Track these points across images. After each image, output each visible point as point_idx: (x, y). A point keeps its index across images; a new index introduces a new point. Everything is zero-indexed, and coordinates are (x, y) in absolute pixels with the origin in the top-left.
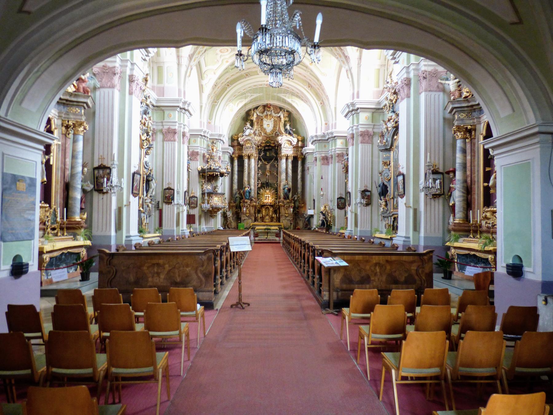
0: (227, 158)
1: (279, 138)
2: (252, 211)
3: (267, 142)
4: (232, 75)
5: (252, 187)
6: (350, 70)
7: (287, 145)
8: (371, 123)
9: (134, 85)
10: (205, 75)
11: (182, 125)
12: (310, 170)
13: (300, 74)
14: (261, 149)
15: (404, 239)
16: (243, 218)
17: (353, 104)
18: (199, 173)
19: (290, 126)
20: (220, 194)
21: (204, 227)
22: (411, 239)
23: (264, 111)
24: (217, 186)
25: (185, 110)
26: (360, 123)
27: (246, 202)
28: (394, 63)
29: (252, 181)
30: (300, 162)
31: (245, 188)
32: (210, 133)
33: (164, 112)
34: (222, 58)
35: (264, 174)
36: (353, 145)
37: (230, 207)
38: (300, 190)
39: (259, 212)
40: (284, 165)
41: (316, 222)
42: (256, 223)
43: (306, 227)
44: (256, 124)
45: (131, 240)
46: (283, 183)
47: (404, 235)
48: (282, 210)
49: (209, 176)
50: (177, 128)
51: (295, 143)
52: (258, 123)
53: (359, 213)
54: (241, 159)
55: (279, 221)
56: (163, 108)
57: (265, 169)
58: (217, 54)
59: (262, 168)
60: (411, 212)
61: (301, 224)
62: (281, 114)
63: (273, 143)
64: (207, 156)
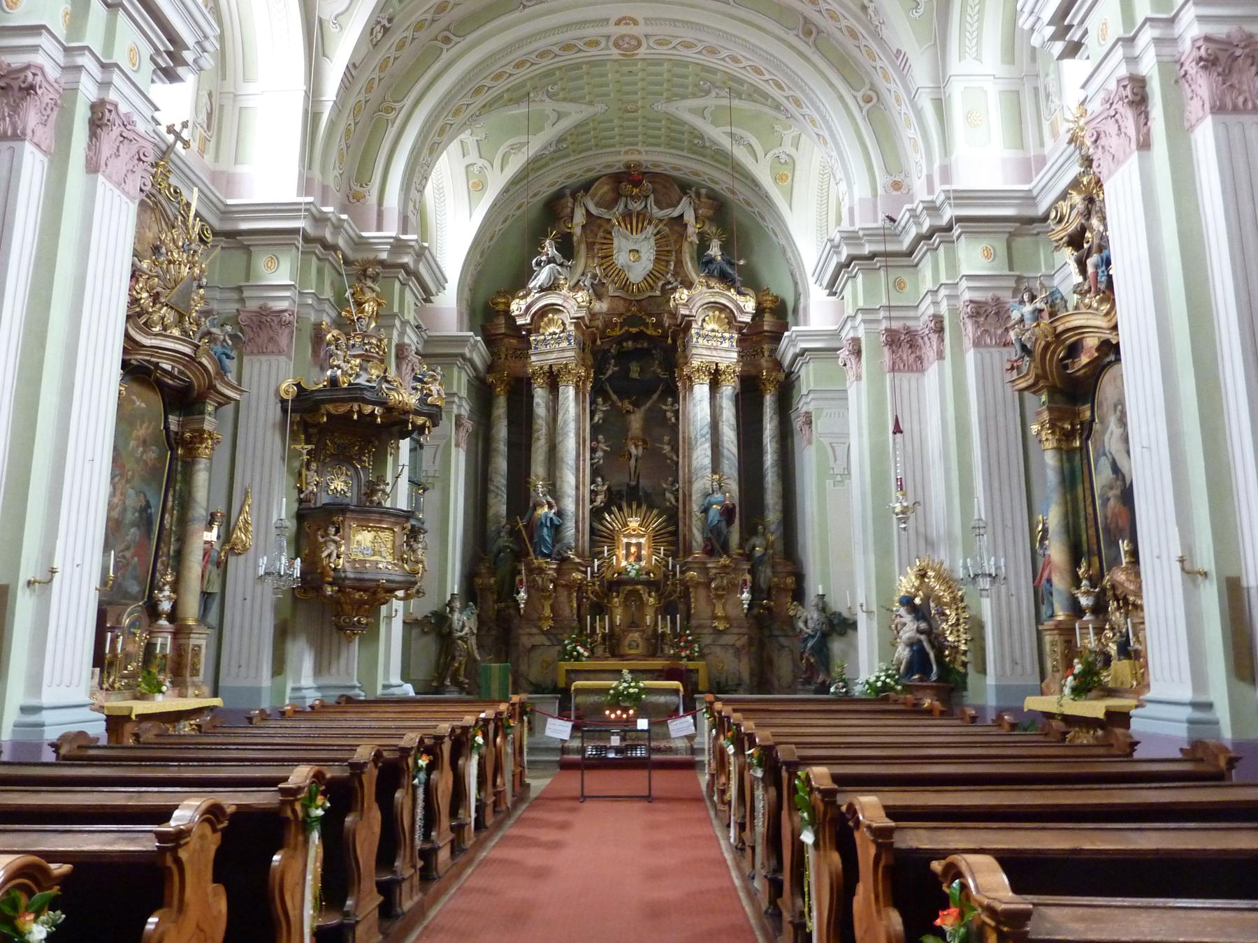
0: (461, 381)
2: (569, 607)
3: (630, 320)
5: (569, 505)
9: (109, 139)
12: (819, 425)
15: (1187, 712)
16: (526, 641)
19: (722, 248)
22: (1222, 712)
23: (615, 202)
27: (541, 571)
29: (571, 486)
31: (535, 509)
33: (249, 254)
35: (617, 453)
36: (1144, 144)
37: (471, 592)
38: (773, 516)
41: (868, 661)
43: (808, 681)
46: (702, 481)
47: (1187, 694)
48: (699, 603)
49: (340, 429)
51: (747, 319)
52: (590, 246)
54: (520, 391)
56: (246, 240)
57: (625, 429)
59: (606, 431)
60: (1210, 597)
61: (784, 667)
63: (656, 326)
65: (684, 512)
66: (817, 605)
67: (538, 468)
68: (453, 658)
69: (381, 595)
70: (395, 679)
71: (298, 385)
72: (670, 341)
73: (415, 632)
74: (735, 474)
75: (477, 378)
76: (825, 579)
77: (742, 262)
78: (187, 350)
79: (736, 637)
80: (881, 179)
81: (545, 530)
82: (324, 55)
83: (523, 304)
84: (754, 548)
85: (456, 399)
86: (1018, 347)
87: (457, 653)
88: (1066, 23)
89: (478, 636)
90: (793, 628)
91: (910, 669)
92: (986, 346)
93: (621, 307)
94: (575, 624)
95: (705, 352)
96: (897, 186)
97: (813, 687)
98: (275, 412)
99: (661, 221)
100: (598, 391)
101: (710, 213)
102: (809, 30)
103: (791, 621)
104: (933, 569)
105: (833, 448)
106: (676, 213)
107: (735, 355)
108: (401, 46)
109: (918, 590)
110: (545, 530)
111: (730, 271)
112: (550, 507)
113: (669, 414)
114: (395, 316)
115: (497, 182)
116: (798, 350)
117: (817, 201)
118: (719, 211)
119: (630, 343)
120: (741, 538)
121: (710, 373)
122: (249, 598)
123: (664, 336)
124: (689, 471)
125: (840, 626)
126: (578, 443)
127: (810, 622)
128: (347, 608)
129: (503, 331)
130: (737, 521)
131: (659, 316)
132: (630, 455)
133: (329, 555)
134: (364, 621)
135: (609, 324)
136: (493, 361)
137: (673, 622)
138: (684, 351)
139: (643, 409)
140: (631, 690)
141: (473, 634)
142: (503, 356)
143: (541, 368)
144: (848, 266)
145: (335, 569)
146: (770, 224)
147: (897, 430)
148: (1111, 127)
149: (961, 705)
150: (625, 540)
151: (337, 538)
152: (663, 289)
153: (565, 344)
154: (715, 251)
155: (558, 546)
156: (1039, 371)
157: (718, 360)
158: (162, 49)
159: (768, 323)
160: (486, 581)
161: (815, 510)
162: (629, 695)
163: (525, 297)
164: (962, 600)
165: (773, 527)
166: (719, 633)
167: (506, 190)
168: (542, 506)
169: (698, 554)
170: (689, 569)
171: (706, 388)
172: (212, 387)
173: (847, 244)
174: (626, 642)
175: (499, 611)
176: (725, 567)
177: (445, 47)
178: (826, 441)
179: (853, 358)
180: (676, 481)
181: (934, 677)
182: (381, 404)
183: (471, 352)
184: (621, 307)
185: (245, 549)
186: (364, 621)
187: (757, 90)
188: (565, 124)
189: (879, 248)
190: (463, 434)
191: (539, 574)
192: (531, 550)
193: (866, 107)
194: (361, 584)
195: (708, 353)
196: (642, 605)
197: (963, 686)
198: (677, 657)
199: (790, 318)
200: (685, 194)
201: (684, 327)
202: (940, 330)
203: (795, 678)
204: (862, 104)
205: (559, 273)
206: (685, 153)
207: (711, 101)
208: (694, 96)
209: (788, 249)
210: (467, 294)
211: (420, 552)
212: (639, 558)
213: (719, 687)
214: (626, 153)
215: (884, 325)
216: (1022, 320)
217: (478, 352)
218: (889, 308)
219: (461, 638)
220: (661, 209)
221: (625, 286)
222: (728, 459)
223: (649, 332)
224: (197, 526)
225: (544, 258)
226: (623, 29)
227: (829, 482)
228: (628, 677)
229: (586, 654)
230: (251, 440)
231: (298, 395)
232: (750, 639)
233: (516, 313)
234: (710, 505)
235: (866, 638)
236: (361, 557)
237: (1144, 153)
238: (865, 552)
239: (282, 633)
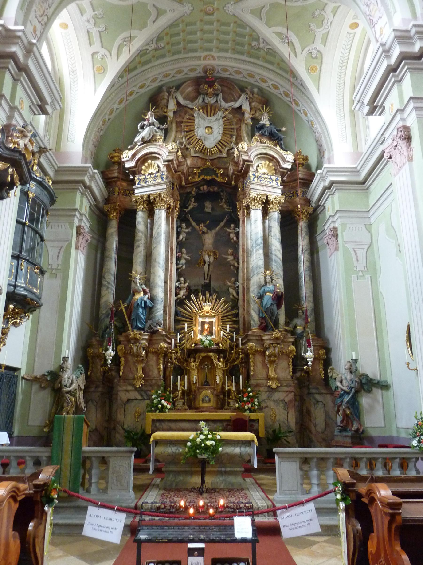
2: (157, 370)
3: (205, 171)
5: (160, 293)
16: (123, 396)
23: (196, 98)
27: (136, 340)
29: (160, 277)
30: (302, 226)
31: (134, 295)
40: (257, 230)
46: (257, 278)
48: (257, 366)
51: (289, 166)
52: (179, 124)
54: (128, 219)
62: (243, 102)
65: (244, 301)
67: (138, 267)
72: (233, 183)
73: (35, 387)
74: (281, 273)
76: (354, 348)
79: (285, 394)
81: (140, 310)
84: (295, 327)
85: (77, 214)
87: (65, 404)
93: (199, 163)
94: (162, 382)
100: (182, 219)
106: (237, 105)
107: (280, 191)
110: (140, 310)
112: (145, 293)
113: (232, 235)
114: (76, 210)
115: (114, 66)
118: (265, 101)
119: (205, 187)
121: (263, 203)
123: (230, 181)
126: (167, 251)
127: (344, 382)
129: (116, 175)
136: (109, 197)
137: (237, 382)
139: (214, 231)
140: (209, 443)
141: (80, 389)
142: (116, 193)
143: (142, 197)
150: (201, 320)
153: (160, 180)
155: (150, 322)
157: (268, 193)
158: (35, 103)
160: (96, 351)
162: (207, 448)
163: (132, 149)
166: (271, 390)
167: (120, 76)
168: (139, 292)
169: (255, 329)
170: (249, 341)
173: (399, 43)
174: (201, 397)
175: (104, 372)
176: (277, 339)
178: (350, 247)
183: (90, 181)
190: (82, 241)
191: (134, 343)
192: (129, 326)
195: (261, 188)
196: (213, 367)
198: (241, 409)
201: (247, 164)
205: (156, 132)
206: (244, 58)
210: (91, 146)
212: (211, 333)
214: (205, 58)
217: (97, 185)
219: (68, 392)
221: (203, 150)
222: (276, 262)
223: (218, 180)
225: (146, 123)
227: (354, 277)
228: (205, 429)
229: (169, 406)
232: (295, 395)
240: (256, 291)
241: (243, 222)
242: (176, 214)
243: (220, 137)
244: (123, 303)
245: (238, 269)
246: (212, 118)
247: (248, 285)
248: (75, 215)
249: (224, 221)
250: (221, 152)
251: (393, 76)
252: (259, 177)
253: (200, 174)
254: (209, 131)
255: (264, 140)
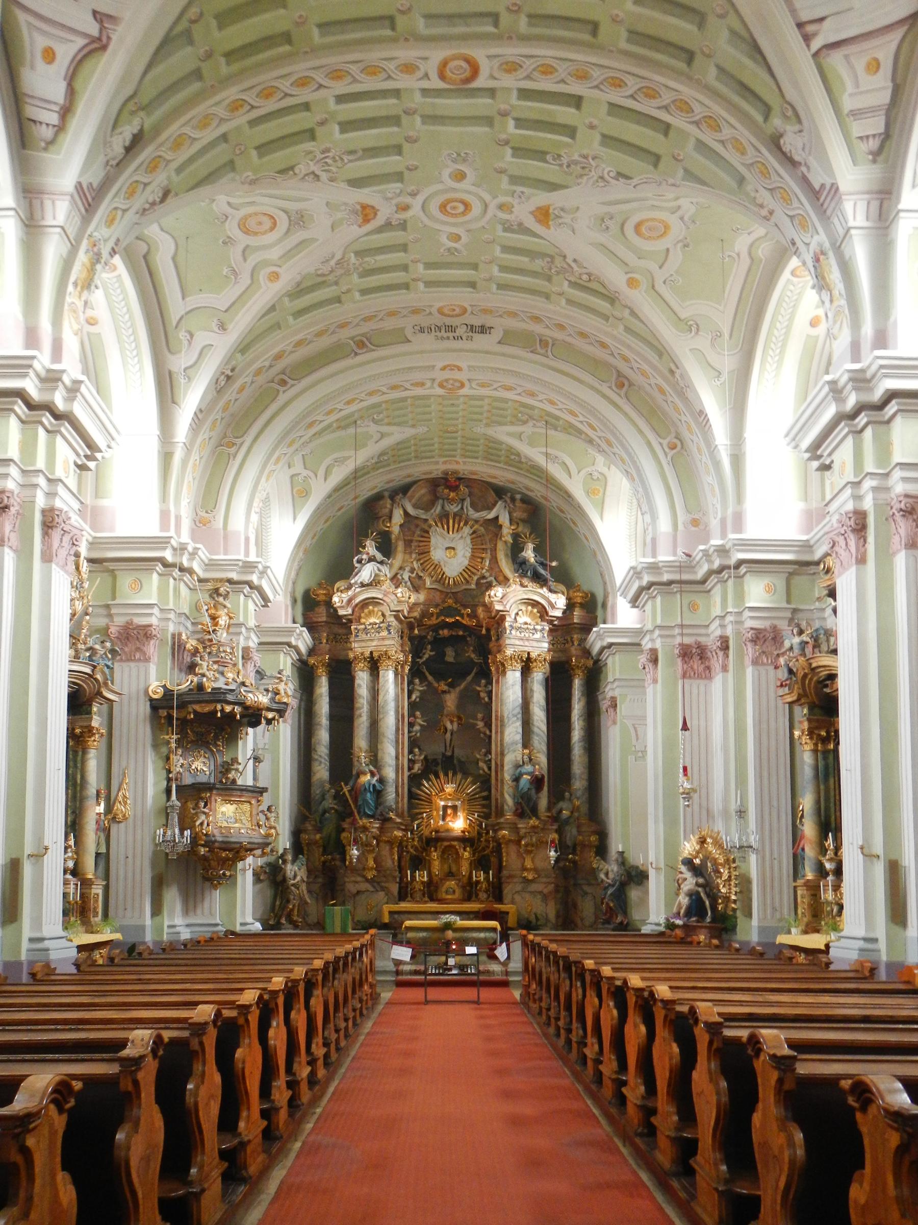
0: (286, 663)
1: (497, 592)
2: (390, 859)
4: (299, 343)
5: (390, 773)
6: (838, 249)
7: (523, 616)
8: (785, 605)
9: (56, 535)
10: (182, 335)
11: (41, 481)
12: (623, 709)
13: (582, 335)
14: (421, 638)
15: (861, 944)
16: (352, 888)
17: (861, 380)
18: (155, 705)
19: (535, 550)
20: (245, 789)
21: (179, 920)
22: (882, 945)
24: (235, 760)
25: (57, 416)
26: (897, 458)
27: (365, 829)
28: (818, 469)
31: (358, 776)
32: (204, 554)
33: (114, 578)
34: (252, 260)
35: (433, 726)
36: (861, 560)
37: (298, 847)
38: (579, 783)
39: (418, 862)
40: (513, 693)
41: (656, 908)
42: (404, 906)
43: (607, 922)
44: (400, 546)
45: (47, 950)
46: (513, 755)
47: (862, 933)
48: (510, 857)
49: (200, 721)
50: (154, 621)
51: (559, 614)
52: (408, 543)
53: (908, 859)
55: (499, 899)
56: (111, 566)
58: (229, 241)
59: (423, 707)
61: (587, 908)
62: (501, 512)
64: (191, 644)
65: (497, 780)
66: (617, 860)
68: (288, 901)
69: (242, 853)
70: (249, 919)
71: (164, 687)
74: (544, 748)
75: (300, 660)
77: (554, 564)
78: (88, 670)
80: (682, 517)
82: (174, 402)
83: (345, 596)
84: (561, 811)
85: (243, 630)
86: (786, 671)
88: (819, 453)
89: (308, 883)
90: (596, 878)
91: (689, 913)
92: (763, 664)
93: (438, 598)
95: (517, 642)
96: (695, 522)
97: (612, 926)
98: (145, 709)
99: (476, 521)
101: (524, 516)
102: (622, 382)
103: (594, 872)
104: (711, 837)
105: (635, 729)
106: (491, 515)
107: (546, 645)
108: (242, 389)
109: (698, 852)
111: (542, 572)
112: (373, 775)
113: (482, 695)
115: (320, 490)
116: (605, 644)
117: (623, 531)
120: (549, 802)
122: (130, 856)
124: (502, 745)
125: (637, 876)
126: (397, 719)
128: (213, 863)
130: (546, 788)
131: (474, 607)
132: (446, 729)
133: (202, 824)
134: (228, 873)
135: (424, 614)
138: (498, 639)
139: (458, 689)
143: (362, 654)
144: (649, 588)
145: (206, 835)
146: (581, 529)
147: (685, 728)
148: (841, 540)
149: (730, 941)
150: (442, 803)
151: (206, 810)
152: (478, 583)
154: (529, 554)
155: (381, 808)
156: (801, 691)
157: (530, 649)
158: (82, 454)
159: (577, 615)
160: (312, 837)
161: (618, 781)
164: (734, 861)
165: (579, 793)
166: (526, 881)
168: (365, 773)
169: (509, 816)
171: (518, 674)
172: (99, 694)
174: (444, 889)
175: (324, 863)
176: (534, 827)
177: (282, 389)
178: (629, 723)
179: (651, 665)
180: (489, 752)
181: (708, 919)
182: (241, 704)
184: (438, 598)
185: (125, 818)
186: (228, 873)
187: (571, 426)
188: (386, 443)
189: (676, 577)
193: (671, 453)
194: (227, 846)
195: (521, 643)
196: (458, 857)
197: (733, 929)
199: (599, 612)
200: (500, 498)
202: (725, 647)
203: (597, 917)
204: (667, 450)
206: (501, 465)
207: (528, 429)
208: (512, 423)
209: (598, 553)
211: (272, 819)
213: (528, 925)
214: (445, 463)
215: (678, 640)
216: (791, 648)
218: (682, 626)
219: (293, 885)
220: (477, 511)
221: (441, 579)
222: (538, 735)
224: (91, 802)
225: (365, 557)
226: (447, 374)
227: (631, 758)
230: (125, 731)
231: (165, 695)
232: (557, 886)
233: (338, 604)
234: (521, 775)
235: (656, 885)
236: (225, 824)
237: (861, 566)
238: (656, 822)
239: (158, 885)
240: (511, 772)
241: (497, 682)
242: (407, 668)
243: (466, 562)
244: (346, 784)
245: (490, 737)
246: (455, 535)
247: (502, 761)
248: (240, 633)
249: (473, 674)
250: (468, 582)
251: (846, 425)
252: (518, 629)
253: (438, 615)
254: (452, 553)
255: (526, 581)
